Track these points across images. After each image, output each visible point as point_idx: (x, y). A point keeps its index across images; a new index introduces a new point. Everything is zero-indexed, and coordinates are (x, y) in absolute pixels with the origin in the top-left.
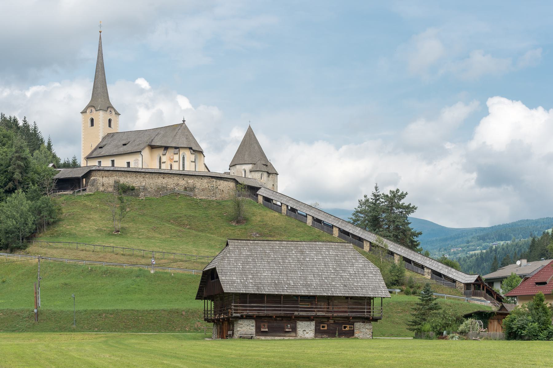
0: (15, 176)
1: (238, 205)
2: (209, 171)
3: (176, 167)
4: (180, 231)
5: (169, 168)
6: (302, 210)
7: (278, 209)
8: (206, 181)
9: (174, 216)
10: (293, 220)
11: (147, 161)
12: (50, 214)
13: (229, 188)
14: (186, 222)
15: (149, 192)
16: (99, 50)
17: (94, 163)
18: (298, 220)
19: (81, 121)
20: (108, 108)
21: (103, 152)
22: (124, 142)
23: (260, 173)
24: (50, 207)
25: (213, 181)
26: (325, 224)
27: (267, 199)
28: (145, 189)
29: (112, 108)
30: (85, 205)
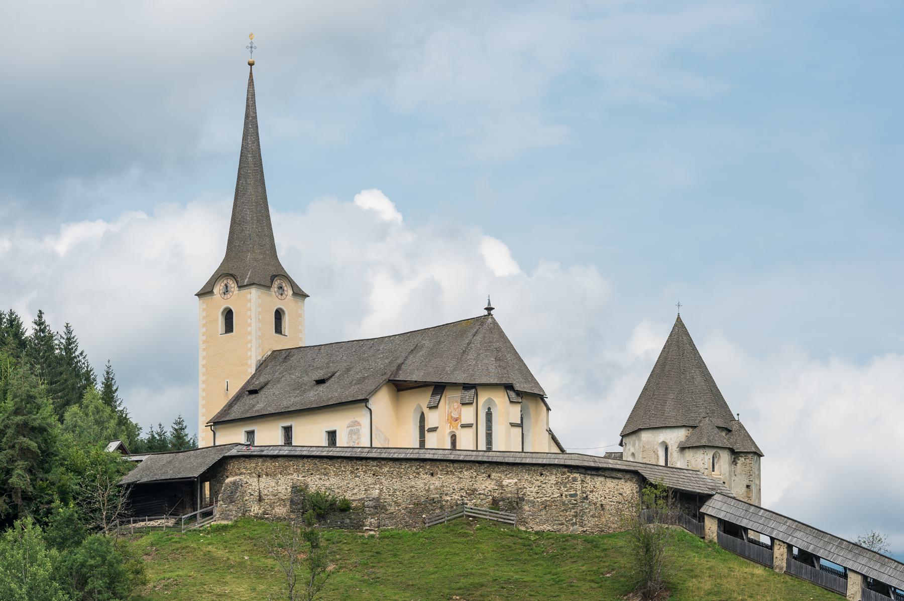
0: (14, 480)
1: (647, 546)
2: (563, 451)
3: (466, 442)
5: (448, 445)
7: (762, 555)
8: (553, 479)
9: (463, 582)
10: (806, 586)
11: (386, 425)
13: (619, 498)
15: (392, 516)
16: (247, 116)
17: (235, 436)
19: (202, 317)
20: (273, 278)
21: (260, 404)
22: (319, 375)
24: (111, 565)
25: (575, 480)
27: (730, 529)
28: (379, 506)
29: (286, 277)
30: (210, 558)
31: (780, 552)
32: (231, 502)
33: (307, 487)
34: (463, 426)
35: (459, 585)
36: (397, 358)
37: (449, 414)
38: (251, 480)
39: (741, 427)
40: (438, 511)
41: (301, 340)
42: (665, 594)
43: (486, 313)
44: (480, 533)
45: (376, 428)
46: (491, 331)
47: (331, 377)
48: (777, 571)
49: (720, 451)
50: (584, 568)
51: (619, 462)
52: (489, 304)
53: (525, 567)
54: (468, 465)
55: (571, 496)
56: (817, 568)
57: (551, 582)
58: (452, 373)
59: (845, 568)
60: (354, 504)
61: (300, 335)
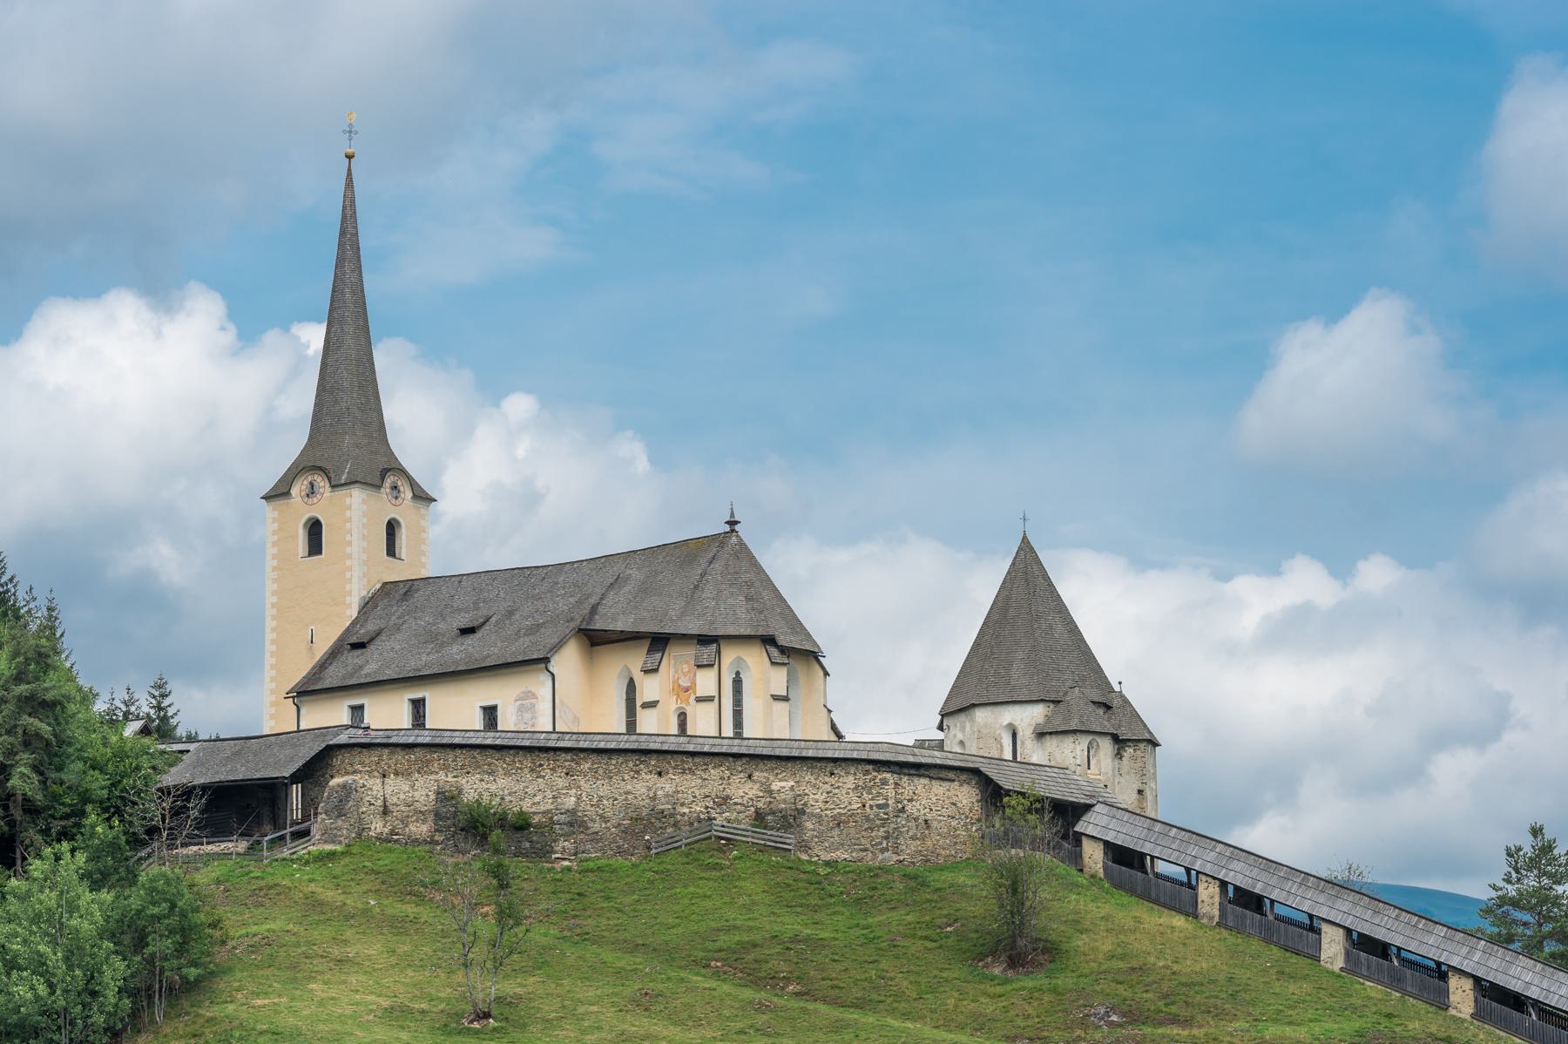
0: (14, 782)
1: (1014, 886)
2: (839, 736)
3: (704, 723)
4: (762, 1008)
5: (674, 730)
6: (1295, 901)
7: (1178, 896)
8: (850, 781)
9: (724, 940)
10: (1255, 945)
11: (573, 697)
12: (181, 949)
13: (952, 811)
14: (784, 969)
15: (595, 837)
16: (343, 232)
17: (331, 715)
18: (1277, 944)
19: (279, 529)
20: (384, 473)
21: (371, 664)
22: (464, 621)
23: (1084, 741)
24: (183, 915)
25: (884, 782)
26: (1404, 961)
27: (1124, 857)
28: (576, 823)
29: (402, 471)
30: (315, 904)
31: (1208, 894)
32: (339, 816)
33: (460, 792)
34: (699, 700)
35: (718, 945)
36: (589, 596)
37: (676, 682)
38: (371, 782)
39: (1126, 701)
40: (670, 830)
41: (423, 566)
42: (1041, 958)
43: (727, 528)
44: (739, 865)
45: (562, 703)
46: (737, 556)
47: (484, 624)
48: (1205, 921)
49: (1098, 739)
50: (909, 918)
51: (936, 753)
52: (732, 515)
53: (817, 917)
54: (717, 760)
55: (879, 806)
56: (1271, 917)
57: (862, 940)
58: (680, 618)
59: (1311, 917)
60: (536, 819)
61: (423, 559)
